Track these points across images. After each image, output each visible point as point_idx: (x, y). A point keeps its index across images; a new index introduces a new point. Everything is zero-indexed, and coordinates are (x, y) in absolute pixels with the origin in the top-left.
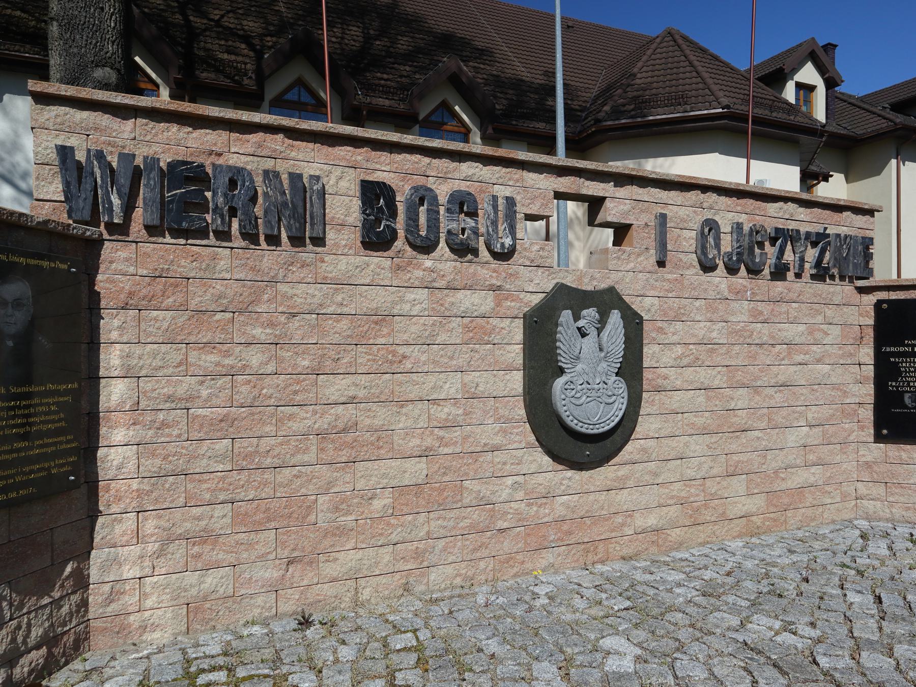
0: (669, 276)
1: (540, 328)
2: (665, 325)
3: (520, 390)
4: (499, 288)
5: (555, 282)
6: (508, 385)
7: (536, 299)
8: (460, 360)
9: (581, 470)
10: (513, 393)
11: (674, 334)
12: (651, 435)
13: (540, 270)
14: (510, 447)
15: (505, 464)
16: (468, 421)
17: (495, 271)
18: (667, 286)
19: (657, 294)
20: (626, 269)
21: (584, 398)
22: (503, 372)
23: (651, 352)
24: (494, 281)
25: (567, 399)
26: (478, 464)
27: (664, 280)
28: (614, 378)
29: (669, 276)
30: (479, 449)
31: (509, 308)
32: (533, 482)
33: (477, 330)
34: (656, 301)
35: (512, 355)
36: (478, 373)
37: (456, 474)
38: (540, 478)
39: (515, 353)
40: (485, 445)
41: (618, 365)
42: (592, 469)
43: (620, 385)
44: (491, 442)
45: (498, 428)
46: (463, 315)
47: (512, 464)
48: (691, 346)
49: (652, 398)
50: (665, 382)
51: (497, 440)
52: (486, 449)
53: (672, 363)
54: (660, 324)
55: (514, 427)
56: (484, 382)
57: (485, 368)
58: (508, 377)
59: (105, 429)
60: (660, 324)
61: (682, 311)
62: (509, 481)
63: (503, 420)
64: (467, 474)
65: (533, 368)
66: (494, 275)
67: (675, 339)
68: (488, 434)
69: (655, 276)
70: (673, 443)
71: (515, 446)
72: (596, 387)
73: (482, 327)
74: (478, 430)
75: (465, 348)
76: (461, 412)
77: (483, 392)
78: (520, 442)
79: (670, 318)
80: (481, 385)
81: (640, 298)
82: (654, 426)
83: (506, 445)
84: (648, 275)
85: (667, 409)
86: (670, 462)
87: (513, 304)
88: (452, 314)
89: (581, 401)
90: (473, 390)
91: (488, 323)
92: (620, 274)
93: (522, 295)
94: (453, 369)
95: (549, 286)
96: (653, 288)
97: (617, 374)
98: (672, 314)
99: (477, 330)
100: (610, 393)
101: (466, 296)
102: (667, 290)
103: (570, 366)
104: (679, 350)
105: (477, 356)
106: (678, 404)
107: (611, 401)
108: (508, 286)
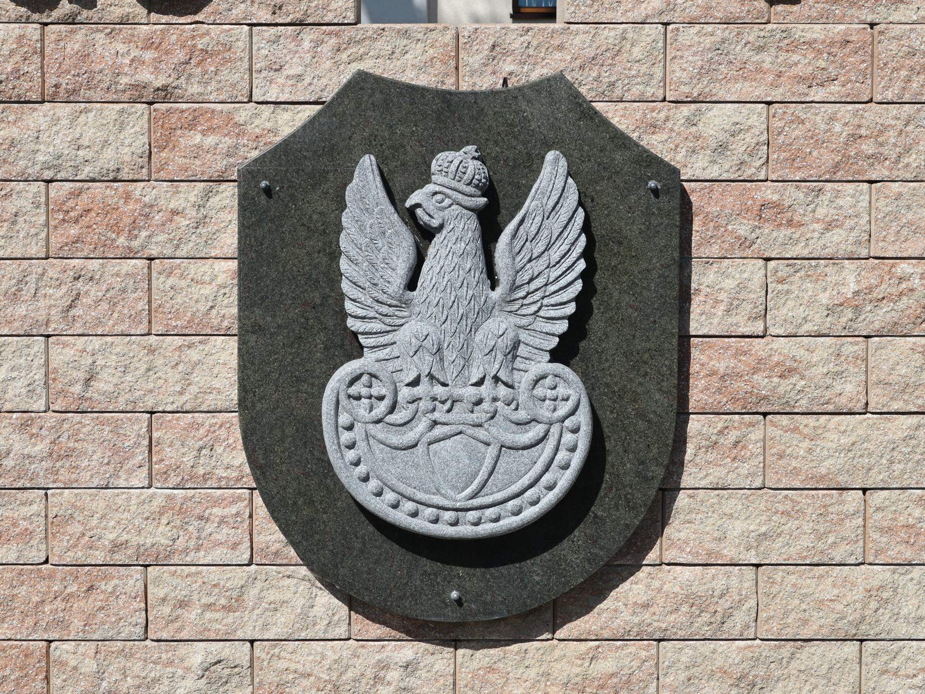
0: (816, 32)
1: (287, 206)
2: (794, 194)
3: (233, 395)
4: (165, 94)
5: (355, 67)
6: (195, 378)
7: (289, 122)
8: (42, 303)
9: (456, 644)
10: (210, 402)
11: (830, 226)
12: (729, 553)
13: (309, 36)
14: (202, 557)
15: (183, 604)
16: (64, 476)
17: (149, 44)
18: (803, 62)
19: (760, 92)
20: (631, 17)
21: (422, 425)
22: (179, 341)
23: (729, 284)
24: (144, 75)
25: (358, 426)
26: (96, 600)
27: (794, 47)
28: (543, 365)
29: (816, 32)
30: (99, 557)
31: (197, 152)
32: (282, 665)
33: (88, 217)
34: (756, 116)
35: (207, 290)
36: (97, 342)
37: (30, 621)
38: (304, 657)
39: (213, 283)
40: (116, 547)
41: (563, 327)
42: (496, 644)
43: (561, 391)
44: (135, 540)
45: (158, 502)
46: (48, 174)
47: (209, 607)
48: (904, 267)
49: (733, 436)
50: (784, 386)
51: (159, 535)
52: (119, 558)
53: (817, 320)
54: (769, 192)
55: (216, 502)
56: (119, 368)
57: (118, 329)
58: (194, 355)
59: (236, 463)
60: (769, 192)
61: (868, 148)
62: (197, 655)
63: (174, 480)
64: (62, 624)
65: (257, 329)
66: (149, 55)
67: (838, 241)
68: (128, 514)
69: (752, 34)
70: (824, 586)
71: (217, 555)
72: (470, 392)
73: (108, 210)
74: (99, 502)
75: (54, 268)
76: (41, 447)
77: (112, 396)
78: (235, 546)
79: (813, 173)
80: (104, 375)
81: (686, 110)
82: (737, 527)
83: (186, 551)
84: (720, 32)
85: (796, 472)
86: (810, 648)
87: (211, 140)
88: (15, 171)
89: (410, 436)
90: (77, 388)
91: (128, 197)
92: (609, 34)
93: (243, 113)
94: (17, 327)
95: (330, 82)
96: (744, 72)
97: (556, 356)
98: (825, 158)
99: (88, 217)
100: (522, 415)
101: (56, 120)
102: (801, 79)
103: (376, 326)
104: (850, 278)
105: (95, 292)
106: (841, 460)
107: (526, 437)
108: (194, 89)
